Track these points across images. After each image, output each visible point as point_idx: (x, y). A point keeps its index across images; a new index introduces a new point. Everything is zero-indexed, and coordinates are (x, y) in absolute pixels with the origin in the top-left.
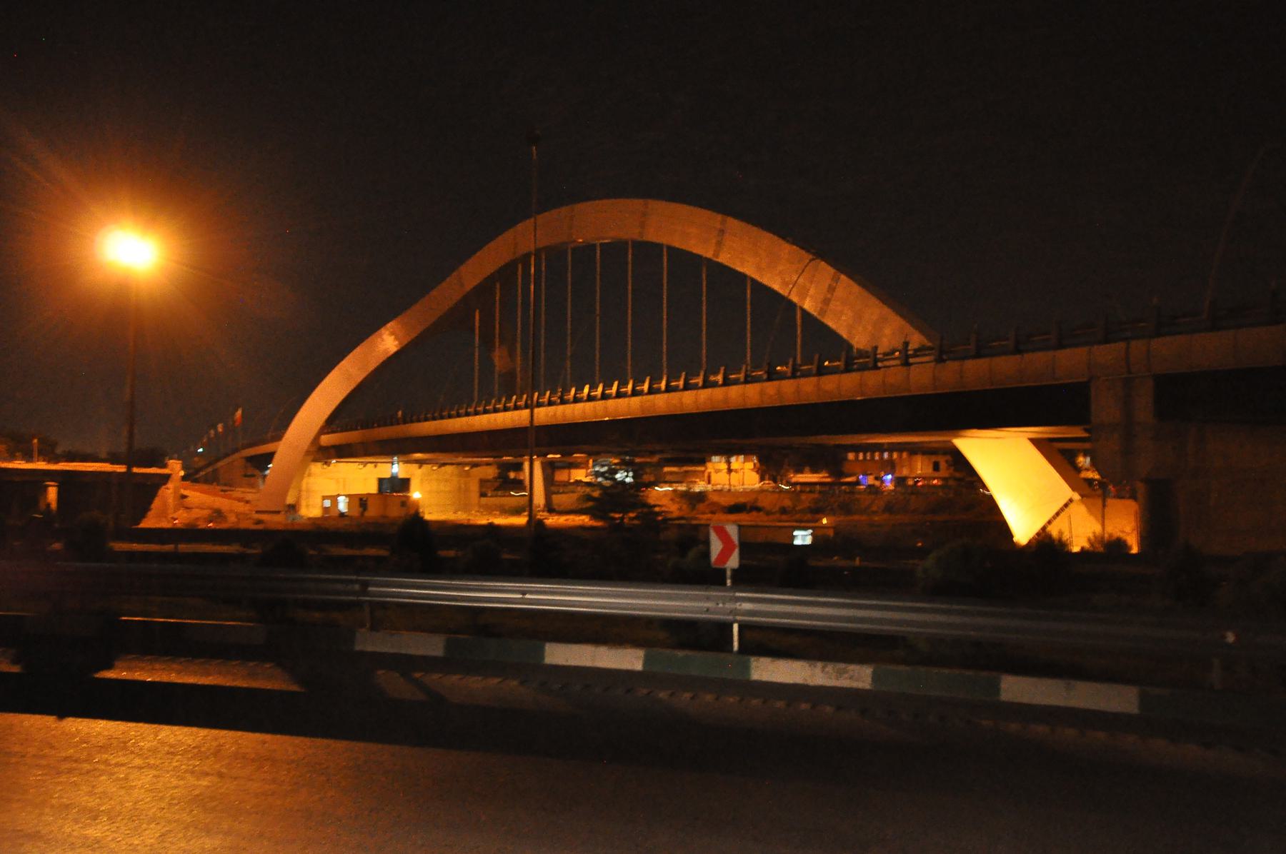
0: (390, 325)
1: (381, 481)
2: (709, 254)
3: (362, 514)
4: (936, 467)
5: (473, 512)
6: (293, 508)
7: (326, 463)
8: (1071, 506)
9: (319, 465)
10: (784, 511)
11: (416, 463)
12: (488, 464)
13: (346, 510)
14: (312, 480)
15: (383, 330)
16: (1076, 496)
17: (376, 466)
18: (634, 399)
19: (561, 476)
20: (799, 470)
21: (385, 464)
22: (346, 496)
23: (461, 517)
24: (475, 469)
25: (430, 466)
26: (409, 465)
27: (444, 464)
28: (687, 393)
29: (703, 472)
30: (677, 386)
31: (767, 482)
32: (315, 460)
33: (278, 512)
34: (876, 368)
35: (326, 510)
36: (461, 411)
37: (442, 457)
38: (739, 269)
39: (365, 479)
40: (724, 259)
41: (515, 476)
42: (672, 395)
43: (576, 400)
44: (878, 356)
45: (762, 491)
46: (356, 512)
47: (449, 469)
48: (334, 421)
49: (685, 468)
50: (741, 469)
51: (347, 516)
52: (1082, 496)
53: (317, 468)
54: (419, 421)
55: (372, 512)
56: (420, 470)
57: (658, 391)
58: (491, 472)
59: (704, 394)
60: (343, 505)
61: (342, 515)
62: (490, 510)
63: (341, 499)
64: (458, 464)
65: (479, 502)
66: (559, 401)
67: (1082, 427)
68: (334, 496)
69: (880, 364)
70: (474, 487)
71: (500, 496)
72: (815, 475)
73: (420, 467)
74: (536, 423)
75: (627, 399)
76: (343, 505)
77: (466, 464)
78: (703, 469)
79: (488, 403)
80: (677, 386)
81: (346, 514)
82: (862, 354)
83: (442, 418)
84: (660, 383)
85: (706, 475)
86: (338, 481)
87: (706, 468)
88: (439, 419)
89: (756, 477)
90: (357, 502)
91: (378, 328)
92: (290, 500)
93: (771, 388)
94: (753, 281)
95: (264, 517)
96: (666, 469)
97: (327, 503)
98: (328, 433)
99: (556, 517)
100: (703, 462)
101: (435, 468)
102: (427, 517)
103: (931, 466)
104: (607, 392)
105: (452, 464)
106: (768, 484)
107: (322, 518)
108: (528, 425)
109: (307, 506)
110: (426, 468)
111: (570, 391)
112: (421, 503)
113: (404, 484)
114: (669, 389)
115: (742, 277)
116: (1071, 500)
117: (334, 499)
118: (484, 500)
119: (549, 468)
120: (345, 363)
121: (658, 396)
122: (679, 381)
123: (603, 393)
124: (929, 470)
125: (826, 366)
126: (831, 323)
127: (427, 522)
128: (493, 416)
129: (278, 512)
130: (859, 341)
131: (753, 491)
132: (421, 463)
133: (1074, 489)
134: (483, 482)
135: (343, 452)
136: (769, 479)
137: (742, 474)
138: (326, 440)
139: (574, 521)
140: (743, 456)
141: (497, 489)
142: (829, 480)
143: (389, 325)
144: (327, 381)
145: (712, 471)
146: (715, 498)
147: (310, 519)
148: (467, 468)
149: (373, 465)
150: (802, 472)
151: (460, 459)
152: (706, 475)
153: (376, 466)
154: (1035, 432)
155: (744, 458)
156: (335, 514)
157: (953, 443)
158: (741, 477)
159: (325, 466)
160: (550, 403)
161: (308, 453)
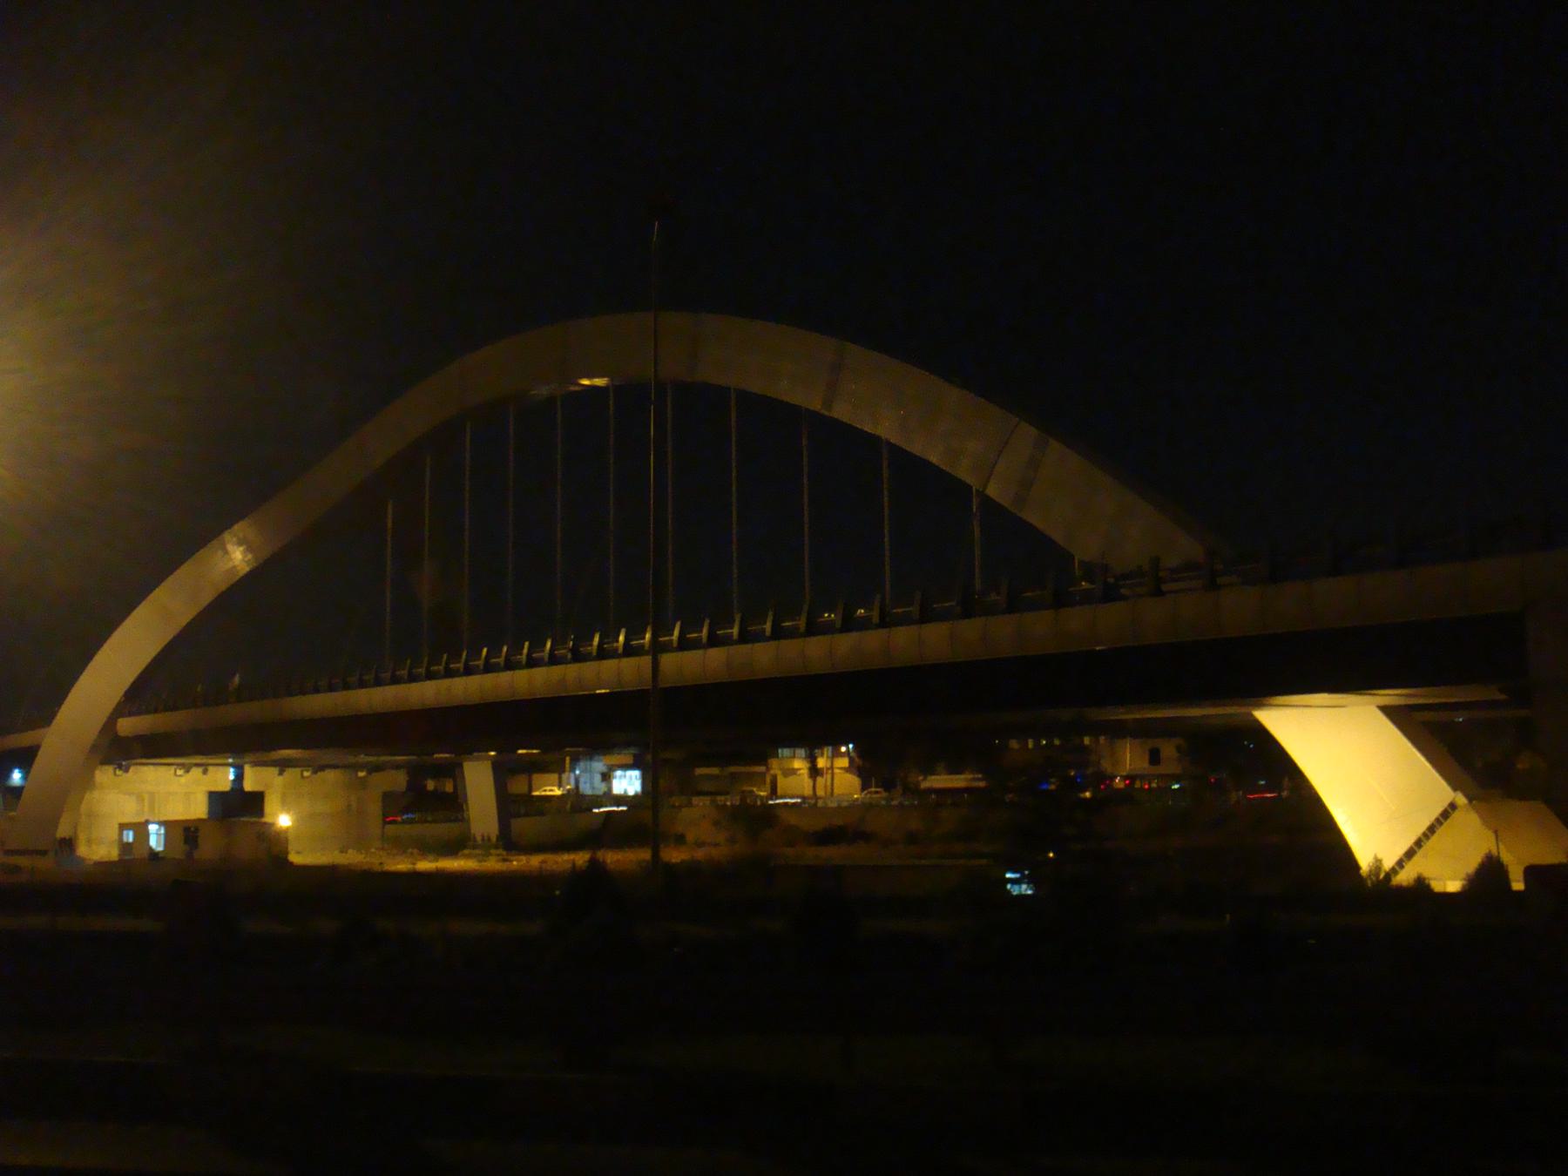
0: (240, 528)
1: (214, 797)
2: (815, 404)
3: (189, 855)
4: (1155, 757)
5: (373, 850)
6: (68, 844)
7: (120, 767)
8: (1456, 815)
9: (109, 769)
10: (912, 838)
11: (275, 766)
12: (397, 767)
13: (160, 849)
14: (96, 794)
15: (227, 536)
16: (1461, 799)
17: (205, 772)
18: (625, 661)
19: (517, 786)
20: (929, 770)
21: (1324, 710)
22: (161, 823)
23: (353, 858)
24: (376, 777)
25: (297, 770)
26: (259, 768)
27: (322, 768)
28: (814, 640)
29: (763, 775)
30: (796, 628)
31: (873, 789)
32: (106, 761)
33: (44, 853)
34: (1158, 593)
35: (125, 848)
36: (366, 677)
37: (328, 756)
38: (868, 428)
39: (187, 794)
40: (841, 411)
41: (436, 787)
42: (784, 643)
43: (603, 654)
44: (1161, 574)
45: (867, 807)
46: (179, 852)
47: (330, 776)
48: (137, 696)
49: (733, 769)
50: (828, 769)
51: (163, 858)
52: (1470, 799)
53: (104, 775)
54: (303, 693)
55: (209, 849)
56: (281, 778)
57: (758, 637)
58: (398, 780)
59: (716, 656)
60: (155, 839)
61: (154, 855)
62: (400, 846)
63: (153, 828)
64: (345, 767)
65: (383, 833)
66: (569, 656)
67: (1391, 696)
68: (139, 824)
69: (1164, 588)
70: (375, 808)
71: (430, 822)
72: (962, 776)
73: (281, 773)
74: (664, 683)
75: (700, 652)
76: (155, 839)
77: (362, 767)
78: (763, 769)
79: (455, 656)
80: (796, 628)
81: (160, 855)
82: (1089, 571)
83: (347, 687)
84: (765, 623)
85: (768, 779)
86: (140, 799)
87: (768, 769)
88: (325, 691)
89: (853, 781)
90: (179, 835)
91: (222, 531)
92: (63, 831)
93: (971, 629)
94: (896, 450)
95: (23, 861)
96: (700, 771)
97: (129, 836)
98: (130, 714)
99: (524, 858)
100: (762, 758)
101: (306, 774)
102: (295, 858)
103: (1147, 757)
104: (534, 655)
105: (335, 767)
106: (877, 795)
107: (121, 862)
108: (648, 686)
109: (89, 841)
110: (292, 773)
111: (592, 639)
112: (291, 837)
113: (254, 803)
114: (778, 634)
115: (873, 441)
116: (1453, 806)
117: (141, 829)
118: (391, 828)
119: (502, 772)
120: (160, 595)
121: (759, 646)
122: (732, 628)
123: (507, 659)
124: (1143, 765)
125: (861, 617)
126: (1033, 517)
127: (675, 865)
128: (444, 684)
129: (44, 853)
130: (1085, 548)
131: (854, 806)
132: (283, 765)
133: (1455, 789)
134: (387, 797)
135: (155, 748)
136: (876, 787)
137: (829, 776)
138: (126, 726)
139: (557, 863)
140: (830, 748)
141: (406, 810)
142: (982, 784)
143: (236, 527)
144: (128, 624)
145: (779, 773)
146: (793, 819)
147: (99, 864)
148: (361, 774)
149: (200, 770)
150: (933, 773)
151: (351, 759)
152: (768, 779)
153: (205, 772)
154: (1397, 695)
155: (833, 749)
156: (139, 853)
157: (1254, 717)
158: (829, 783)
159: (118, 772)
160: (554, 660)
161: (94, 748)
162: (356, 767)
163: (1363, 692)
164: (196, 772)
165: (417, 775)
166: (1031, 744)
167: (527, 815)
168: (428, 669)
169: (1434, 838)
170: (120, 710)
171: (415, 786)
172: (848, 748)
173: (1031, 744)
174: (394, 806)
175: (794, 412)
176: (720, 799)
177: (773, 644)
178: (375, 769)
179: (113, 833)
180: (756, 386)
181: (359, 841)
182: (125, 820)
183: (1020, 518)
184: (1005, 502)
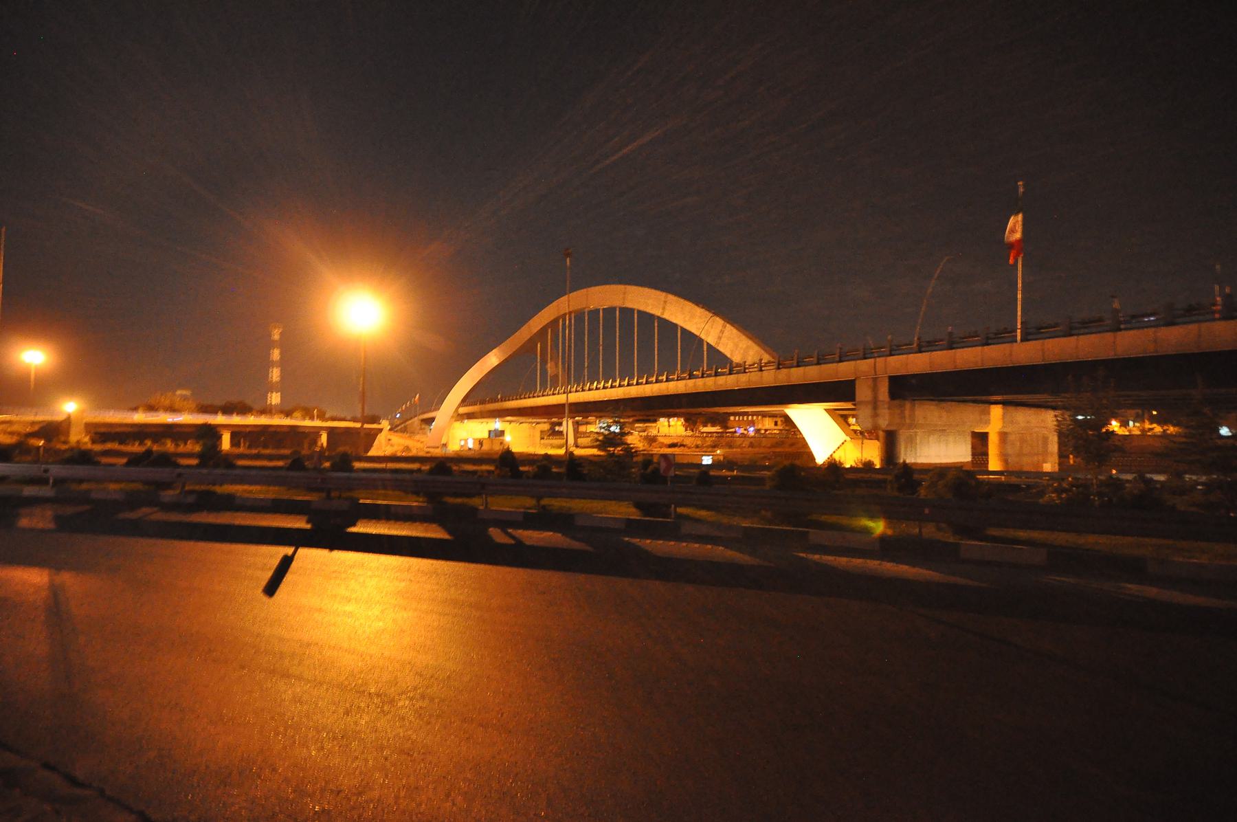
4: (776, 424)
8: (845, 443)
12: (545, 423)
19: (582, 429)
29: (655, 427)
32: (456, 420)
33: (438, 447)
40: (666, 316)
47: (524, 425)
48: (466, 401)
53: (457, 425)
55: (486, 447)
58: (546, 427)
64: (530, 423)
70: (538, 435)
75: (835, 365)
79: (530, 393)
82: (738, 365)
92: (444, 441)
93: (691, 382)
95: (431, 450)
96: (636, 425)
110: (513, 424)
113: (502, 433)
117: (466, 441)
119: (577, 424)
126: (721, 349)
129: (438, 447)
130: (736, 359)
132: (510, 422)
134: (542, 432)
135: (470, 416)
138: (462, 410)
141: (549, 435)
151: (530, 420)
161: (452, 417)
162: (532, 423)
163: (130, 429)
164: (484, 424)
165: (554, 425)
166: (745, 419)
167: (583, 437)
168: (637, 382)
169: (839, 450)
170: (460, 406)
171: (552, 429)
172: (735, 419)
173: (745, 419)
174: (543, 435)
175: (652, 316)
176: (641, 434)
177: (636, 387)
178: (538, 423)
179: (458, 441)
180: (642, 308)
181: (534, 444)
182: (461, 438)
183: (718, 350)
184: (713, 344)
